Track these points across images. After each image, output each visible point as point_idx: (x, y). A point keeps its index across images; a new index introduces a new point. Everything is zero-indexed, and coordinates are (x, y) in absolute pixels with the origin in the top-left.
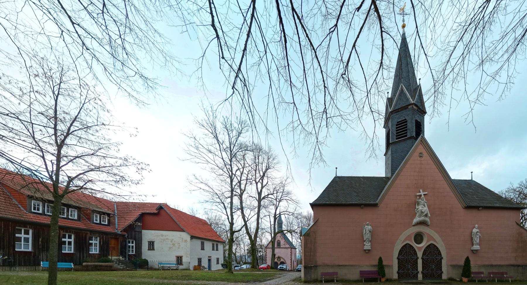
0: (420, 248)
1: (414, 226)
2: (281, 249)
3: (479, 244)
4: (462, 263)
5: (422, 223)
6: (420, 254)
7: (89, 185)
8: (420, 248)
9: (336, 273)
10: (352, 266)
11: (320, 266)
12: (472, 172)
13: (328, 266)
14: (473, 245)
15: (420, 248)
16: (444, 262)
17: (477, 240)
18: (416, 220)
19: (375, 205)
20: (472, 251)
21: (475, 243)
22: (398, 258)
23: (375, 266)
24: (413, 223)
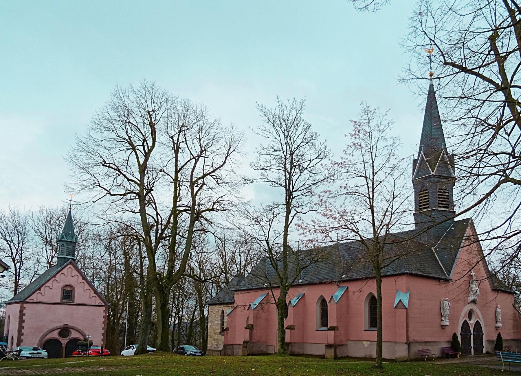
0: (472, 324)
1: (469, 303)
2: (74, 307)
3: (502, 323)
4: (495, 338)
5: (474, 302)
6: (64, 346)
7: (71, 168)
8: (472, 322)
9: (428, 351)
10: (434, 342)
11: (403, 343)
12: (414, 155)
13: (418, 342)
14: (496, 322)
15: (472, 322)
16: (484, 336)
17: (500, 318)
18: (472, 298)
19: (447, 281)
20: (442, 326)
21: (499, 321)
22: (461, 334)
23: (448, 342)
24: (469, 301)
